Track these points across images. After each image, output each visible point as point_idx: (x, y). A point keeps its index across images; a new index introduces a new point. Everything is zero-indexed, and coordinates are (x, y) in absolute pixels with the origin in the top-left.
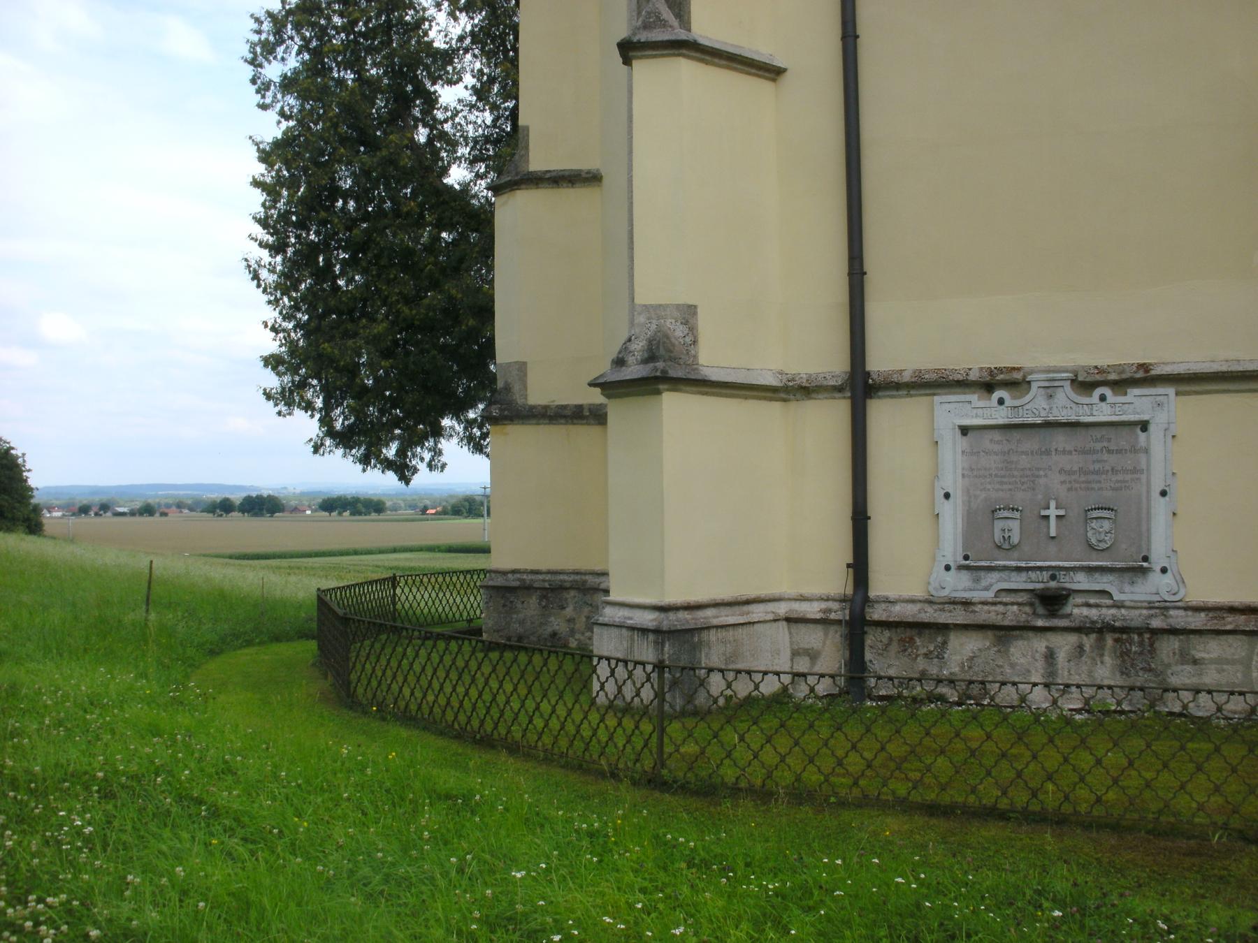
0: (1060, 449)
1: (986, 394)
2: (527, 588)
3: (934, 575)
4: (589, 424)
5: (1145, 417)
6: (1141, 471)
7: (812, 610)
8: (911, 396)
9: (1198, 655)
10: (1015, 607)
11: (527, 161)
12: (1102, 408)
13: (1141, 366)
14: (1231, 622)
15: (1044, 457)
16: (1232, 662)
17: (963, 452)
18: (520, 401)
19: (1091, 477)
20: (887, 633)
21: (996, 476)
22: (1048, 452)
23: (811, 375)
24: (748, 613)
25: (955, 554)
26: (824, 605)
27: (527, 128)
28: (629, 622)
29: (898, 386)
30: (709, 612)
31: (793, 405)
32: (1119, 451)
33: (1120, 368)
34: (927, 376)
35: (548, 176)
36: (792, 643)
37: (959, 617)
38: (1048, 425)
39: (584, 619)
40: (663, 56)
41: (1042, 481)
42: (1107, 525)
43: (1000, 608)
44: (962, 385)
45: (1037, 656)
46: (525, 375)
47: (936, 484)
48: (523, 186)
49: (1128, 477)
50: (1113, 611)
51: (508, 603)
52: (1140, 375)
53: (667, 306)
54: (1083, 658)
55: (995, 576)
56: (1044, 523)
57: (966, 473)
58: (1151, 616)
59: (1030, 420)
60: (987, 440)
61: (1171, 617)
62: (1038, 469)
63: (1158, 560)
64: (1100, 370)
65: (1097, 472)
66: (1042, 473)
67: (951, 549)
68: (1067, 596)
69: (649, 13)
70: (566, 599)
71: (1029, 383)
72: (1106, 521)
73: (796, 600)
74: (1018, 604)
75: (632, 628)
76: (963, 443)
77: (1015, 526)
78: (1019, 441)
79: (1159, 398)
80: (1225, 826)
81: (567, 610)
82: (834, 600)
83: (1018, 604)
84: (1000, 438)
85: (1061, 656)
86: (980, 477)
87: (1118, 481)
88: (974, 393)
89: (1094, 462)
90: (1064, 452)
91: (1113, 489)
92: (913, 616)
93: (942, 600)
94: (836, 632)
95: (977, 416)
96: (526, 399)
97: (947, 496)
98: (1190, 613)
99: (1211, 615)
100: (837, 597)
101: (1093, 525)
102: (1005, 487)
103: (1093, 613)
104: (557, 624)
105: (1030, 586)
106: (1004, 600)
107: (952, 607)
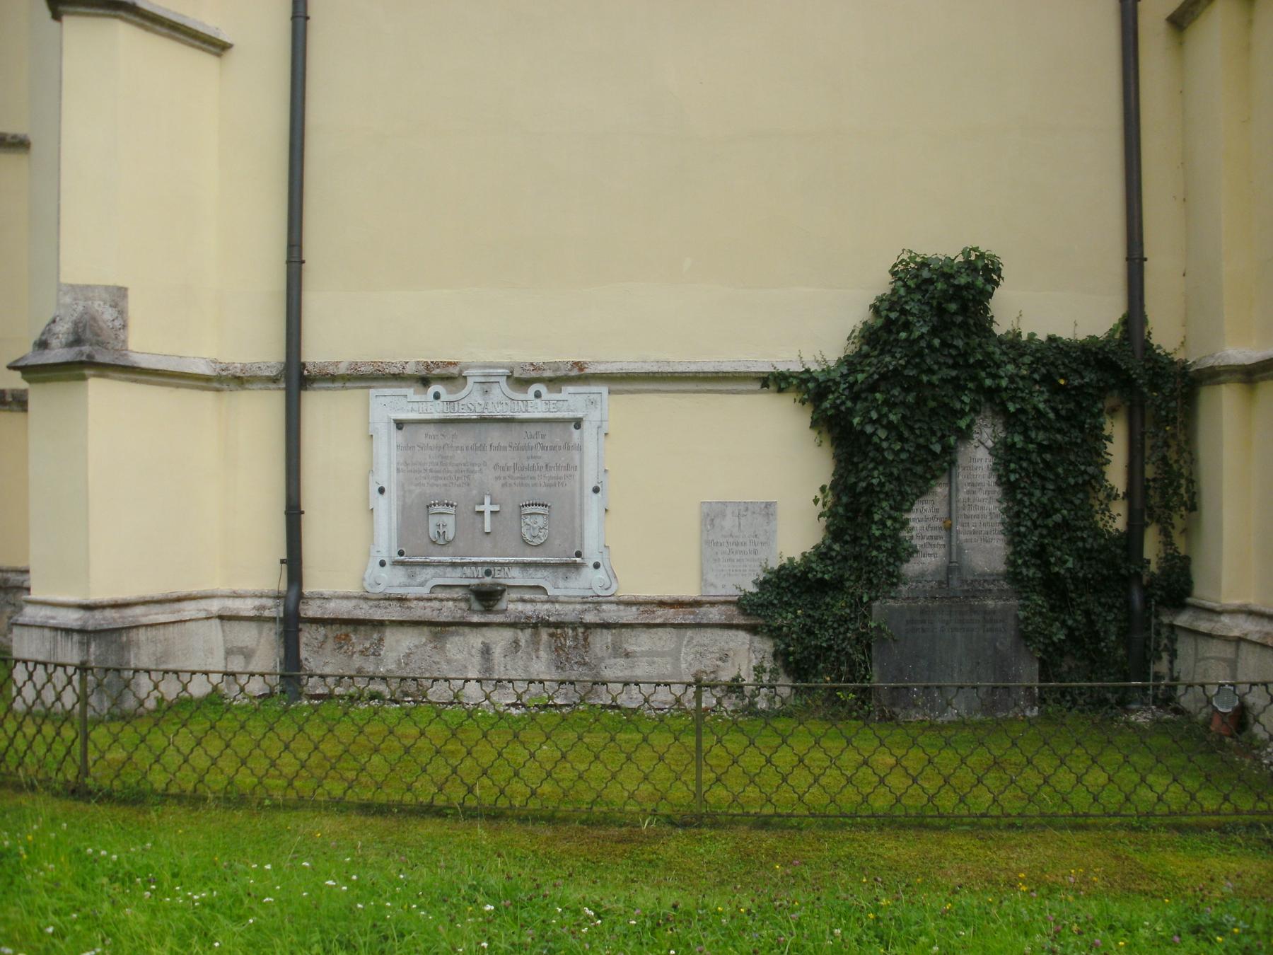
0: (495, 444)
1: (421, 388)
3: (369, 571)
5: (579, 415)
6: (575, 468)
7: (246, 607)
8: (347, 388)
9: (630, 648)
10: (451, 603)
12: (537, 405)
13: (575, 364)
14: (661, 615)
15: (479, 452)
16: (662, 654)
17: (398, 446)
19: (526, 473)
20: (322, 630)
21: (431, 471)
22: (482, 448)
23: (245, 365)
26: (257, 602)
28: (52, 622)
29: (333, 378)
30: (138, 611)
32: (553, 448)
33: (556, 366)
34: (363, 369)
36: (225, 641)
37: (394, 613)
38: (483, 420)
41: (477, 476)
42: (540, 521)
43: (436, 604)
45: (474, 651)
49: (562, 473)
50: (547, 606)
52: (575, 372)
56: (478, 518)
57: (401, 467)
59: (466, 415)
60: (422, 434)
62: (473, 465)
63: (591, 556)
65: (531, 469)
67: (386, 545)
68: (503, 592)
71: (465, 377)
73: (228, 597)
74: (454, 600)
75: (55, 629)
77: (450, 521)
79: (592, 397)
82: (268, 597)
83: (454, 600)
84: (435, 433)
85: (497, 652)
86: (415, 471)
88: (410, 387)
89: (528, 458)
90: (499, 448)
92: (349, 612)
93: (375, 597)
94: (271, 630)
95: (412, 410)
97: (382, 491)
98: (622, 607)
102: (440, 482)
103: (528, 609)
106: (440, 596)
107: (387, 603)
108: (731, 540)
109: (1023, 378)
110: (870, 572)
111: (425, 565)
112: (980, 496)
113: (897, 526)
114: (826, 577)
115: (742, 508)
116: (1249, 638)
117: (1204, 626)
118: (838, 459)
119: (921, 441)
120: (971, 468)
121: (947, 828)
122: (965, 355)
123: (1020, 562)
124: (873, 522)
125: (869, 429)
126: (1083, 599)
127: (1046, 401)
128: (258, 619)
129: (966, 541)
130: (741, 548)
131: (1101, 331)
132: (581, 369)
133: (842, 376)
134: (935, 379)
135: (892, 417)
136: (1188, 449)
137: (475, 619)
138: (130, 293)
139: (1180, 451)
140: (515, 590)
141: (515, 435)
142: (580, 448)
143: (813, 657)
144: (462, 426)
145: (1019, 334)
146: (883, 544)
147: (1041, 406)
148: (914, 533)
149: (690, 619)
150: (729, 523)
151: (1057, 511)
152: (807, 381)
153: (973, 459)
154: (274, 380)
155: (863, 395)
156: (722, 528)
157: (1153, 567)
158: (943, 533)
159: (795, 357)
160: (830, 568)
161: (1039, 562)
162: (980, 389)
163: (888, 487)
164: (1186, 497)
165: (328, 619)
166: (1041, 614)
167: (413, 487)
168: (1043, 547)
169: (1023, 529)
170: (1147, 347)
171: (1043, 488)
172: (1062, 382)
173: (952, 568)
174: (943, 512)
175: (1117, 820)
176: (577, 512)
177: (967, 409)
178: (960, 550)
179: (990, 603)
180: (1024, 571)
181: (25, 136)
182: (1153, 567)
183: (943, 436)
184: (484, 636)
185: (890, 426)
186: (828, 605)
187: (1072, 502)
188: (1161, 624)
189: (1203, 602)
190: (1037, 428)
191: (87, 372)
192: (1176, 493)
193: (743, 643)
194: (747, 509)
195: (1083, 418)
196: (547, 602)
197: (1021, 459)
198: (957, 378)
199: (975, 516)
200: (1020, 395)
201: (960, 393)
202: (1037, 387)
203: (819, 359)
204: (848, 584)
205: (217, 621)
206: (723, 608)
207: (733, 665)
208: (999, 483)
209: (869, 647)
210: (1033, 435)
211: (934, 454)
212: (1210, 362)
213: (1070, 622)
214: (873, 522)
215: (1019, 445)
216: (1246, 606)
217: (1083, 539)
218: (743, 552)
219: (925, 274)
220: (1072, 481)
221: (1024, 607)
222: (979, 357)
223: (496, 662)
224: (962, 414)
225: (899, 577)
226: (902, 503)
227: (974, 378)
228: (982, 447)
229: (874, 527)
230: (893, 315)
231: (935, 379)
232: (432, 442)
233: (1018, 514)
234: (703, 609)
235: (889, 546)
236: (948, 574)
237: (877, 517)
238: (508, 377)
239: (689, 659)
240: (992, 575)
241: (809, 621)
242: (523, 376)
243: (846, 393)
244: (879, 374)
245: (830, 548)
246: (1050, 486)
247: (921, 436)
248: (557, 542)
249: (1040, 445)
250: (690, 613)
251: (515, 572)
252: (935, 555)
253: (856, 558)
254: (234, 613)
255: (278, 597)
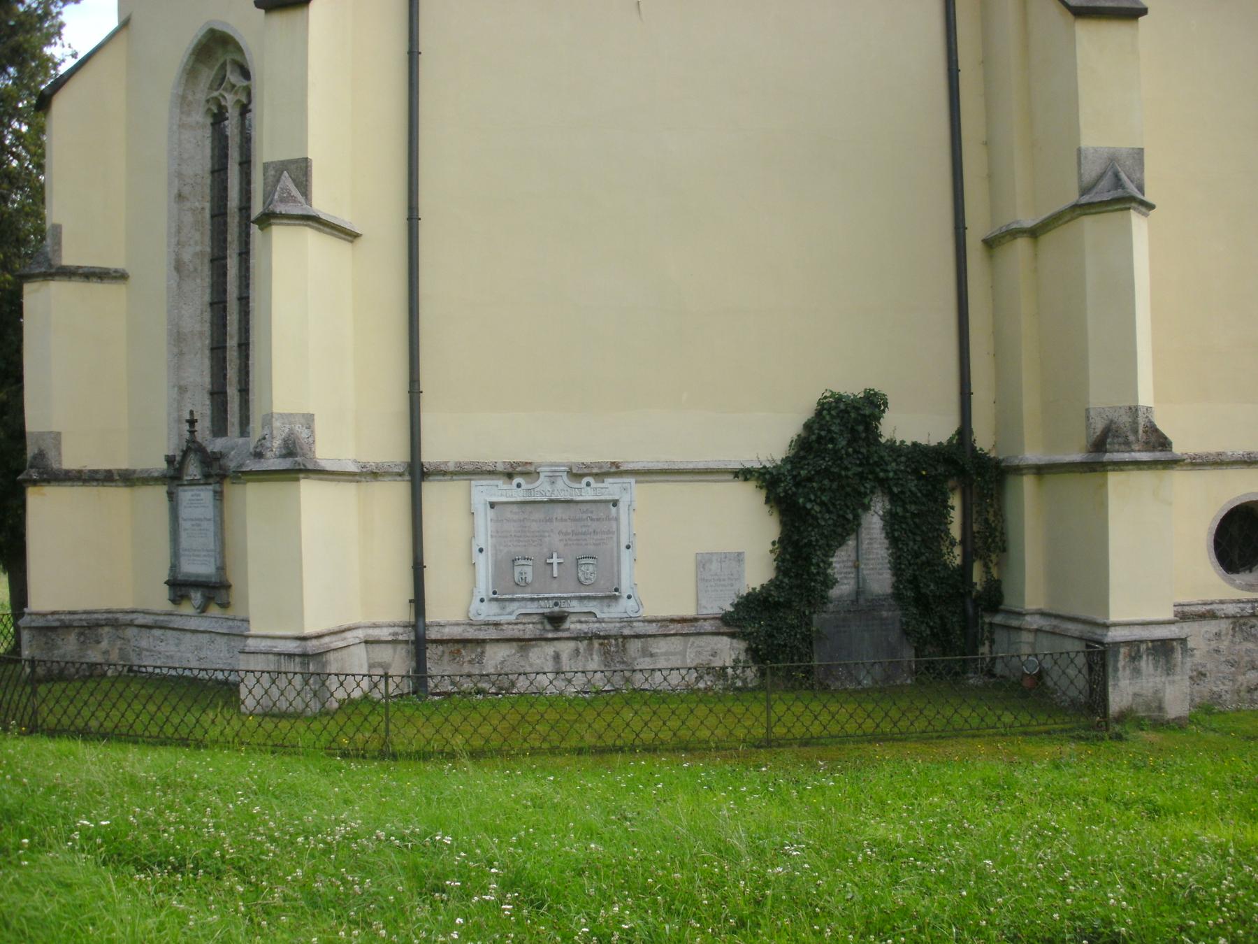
2: (66, 627)
4: (116, 486)
5: (616, 498)
6: (613, 533)
7: (384, 634)
8: (453, 480)
9: (654, 651)
10: (531, 625)
11: (60, 257)
12: (588, 491)
13: (613, 463)
14: (673, 628)
16: (674, 654)
18: (55, 466)
20: (441, 648)
22: (550, 520)
23: (378, 464)
24: (345, 639)
25: (487, 590)
26: (391, 630)
27: (57, 229)
28: (276, 650)
29: (445, 473)
30: (326, 640)
31: (364, 485)
32: (598, 520)
33: (600, 465)
35: (80, 271)
36: (368, 659)
37: (492, 634)
38: (551, 501)
39: (117, 651)
40: (295, 225)
41: (547, 539)
42: (591, 568)
43: (521, 627)
44: (492, 473)
45: (548, 658)
46: (60, 443)
47: (473, 542)
48: (57, 278)
50: (597, 625)
51: (50, 641)
52: (613, 470)
53: (297, 414)
54: (580, 657)
55: (516, 605)
56: (548, 568)
58: (622, 627)
59: (539, 498)
60: (509, 513)
61: (635, 627)
62: (544, 531)
63: (625, 590)
64: (587, 466)
66: (547, 534)
67: (484, 586)
69: (282, 189)
70: (102, 634)
71: (538, 473)
72: (591, 566)
73: (369, 627)
74: (533, 623)
75: (279, 654)
76: (491, 513)
77: (529, 570)
78: (531, 512)
79: (624, 485)
80: (744, 741)
81: (103, 643)
82: (399, 626)
83: (533, 623)
84: (517, 510)
85: (565, 658)
87: (596, 540)
88: (499, 479)
89: (581, 527)
90: (562, 520)
91: (594, 544)
92: (460, 635)
93: (479, 623)
94: (402, 649)
95: (502, 495)
96: (60, 463)
97: (481, 550)
98: (646, 624)
99: (659, 624)
100: (401, 624)
101: (582, 568)
102: (521, 543)
103: (584, 627)
104: (94, 656)
105: (540, 611)
106: (523, 621)
107: (486, 627)
108: (716, 578)
109: (901, 471)
110: (808, 596)
111: (512, 600)
112: (876, 546)
113: (826, 566)
114: (781, 600)
115: (723, 556)
116: (1044, 629)
117: (1015, 623)
118: (783, 524)
119: (841, 512)
120: (869, 528)
121: (905, 740)
122: (867, 458)
123: (901, 587)
124: (812, 564)
125: (809, 506)
126: (939, 609)
127: (916, 486)
128: (394, 642)
129: (867, 574)
130: (722, 583)
131: (944, 439)
132: (618, 467)
133: (788, 471)
134: (850, 473)
135: (824, 498)
136: (1000, 513)
137: (550, 635)
138: (316, 417)
139: (995, 515)
140: (574, 615)
141: (573, 511)
142: (617, 519)
143: (774, 652)
144: (536, 505)
145: (895, 442)
146: (818, 578)
147: (913, 489)
148: (836, 570)
149: (692, 630)
150: (714, 566)
151: (923, 554)
152: (765, 474)
153: (870, 523)
154: (400, 475)
155: (803, 484)
156: (710, 570)
157: (979, 588)
158: (853, 570)
159: (754, 458)
160: (783, 594)
161: (912, 586)
162: (877, 479)
163: (821, 542)
164: (1000, 544)
165: (446, 640)
166: (915, 619)
167: (502, 548)
168: (915, 577)
169: (903, 566)
170: (974, 449)
171: (915, 541)
172: (924, 473)
173: (859, 592)
174: (853, 557)
175: (994, 731)
176: (615, 561)
177: (868, 492)
178: (864, 580)
179: (885, 614)
180: (904, 592)
181: (123, 270)
182: (979, 588)
183: (854, 509)
184: (554, 647)
185: (822, 504)
186: (781, 618)
187: (931, 548)
188: (984, 623)
189: (1013, 608)
190: (910, 503)
191: (301, 476)
192: (993, 541)
193: (727, 645)
194: (726, 557)
195: (936, 495)
196: (596, 622)
197: (901, 522)
198: (862, 472)
199: (874, 559)
200: (901, 482)
201: (864, 482)
202: (910, 477)
203: (770, 459)
204: (795, 604)
205: (363, 645)
206: (712, 622)
207: (720, 659)
208: (887, 537)
209: (811, 643)
210: (908, 507)
211: (848, 520)
212: (1016, 462)
213: (932, 624)
214: (812, 564)
215: (901, 514)
216: (1039, 610)
217: (938, 571)
218: (724, 586)
219: (842, 406)
220: (930, 535)
221: (904, 615)
222: (876, 459)
223: (564, 664)
224: (866, 494)
225: (827, 598)
226: (829, 550)
227: (872, 472)
228: (876, 515)
229: (812, 568)
230: (823, 433)
231: (850, 473)
232: (516, 517)
233: (899, 557)
234: (700, 623)
235: (822, 579)
236: (857, 596)
237: (814, 561)
238: (568, 472)
239: (692, 656)
240: (883, 595)
241: (769, 629)
242: (579, 472)
243: (791, 482)
244: (815, 471)
245: (782, 582)
246: (918, 538)
247: (841, 509)
248: (602, 582)
249: (913, 513)
250: (692, 626)
251: (575, 603)
252: (848, 584)
253: (799, 587)
254: (376, 638)
255: (406, 627)
